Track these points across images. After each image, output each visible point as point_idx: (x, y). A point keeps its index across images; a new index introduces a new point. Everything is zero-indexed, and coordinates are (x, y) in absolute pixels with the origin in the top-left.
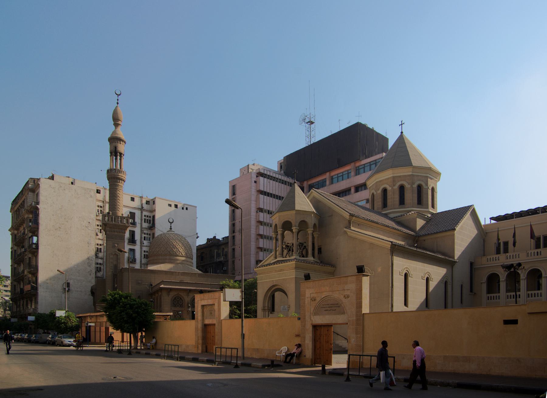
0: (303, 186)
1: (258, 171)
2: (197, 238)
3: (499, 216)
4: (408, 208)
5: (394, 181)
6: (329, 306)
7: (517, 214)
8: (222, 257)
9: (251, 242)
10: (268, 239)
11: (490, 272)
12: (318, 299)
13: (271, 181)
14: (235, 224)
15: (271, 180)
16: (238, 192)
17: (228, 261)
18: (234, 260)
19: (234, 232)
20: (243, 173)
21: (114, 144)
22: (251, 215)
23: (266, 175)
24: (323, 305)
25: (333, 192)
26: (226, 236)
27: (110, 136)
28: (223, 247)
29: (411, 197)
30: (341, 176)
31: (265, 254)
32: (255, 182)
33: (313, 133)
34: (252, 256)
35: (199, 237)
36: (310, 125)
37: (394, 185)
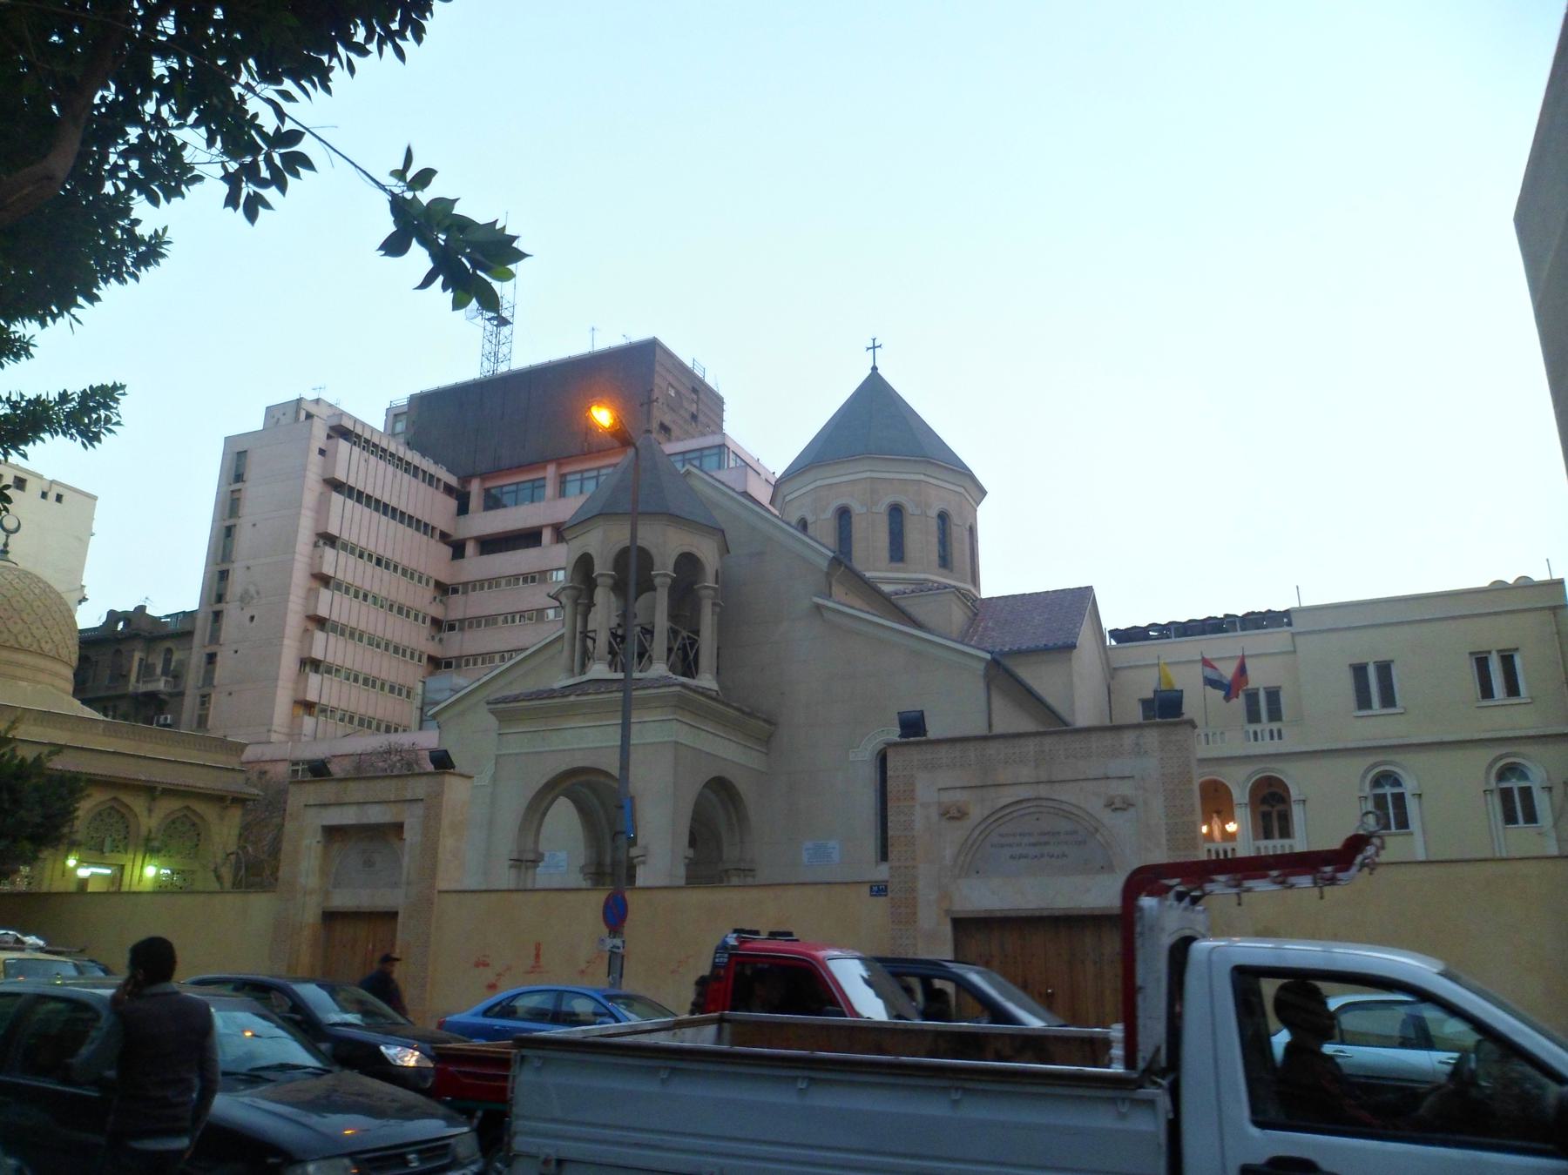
0: (468, 490)
1: (334, 422)
2: (80, 602)
3: (1210, 618)
4: (915, 572)
6: (1032, 840)
7: (1216, 624)
8: (163, 679)
9: (283, 637)
10: (342, 634)
11: (1265, 772)
12: (976, 813)
13: (373, 459)
14: (231, 572)
15: (372, 454)
16: (252, 473)
17: (181, 694)
18: (209, 695)
19: (220, 598)
20: (275, 419)
22: (294, 552)
23: (358, 436)
24: (1001, 835)
26: (187, 610)
28: (168, 644)
30: (513, 492)
31: (327, 683)
32: (322, 452)
33: (504, 350)
34: (280, 683)
35: (87, 599)
36: (497, 326)
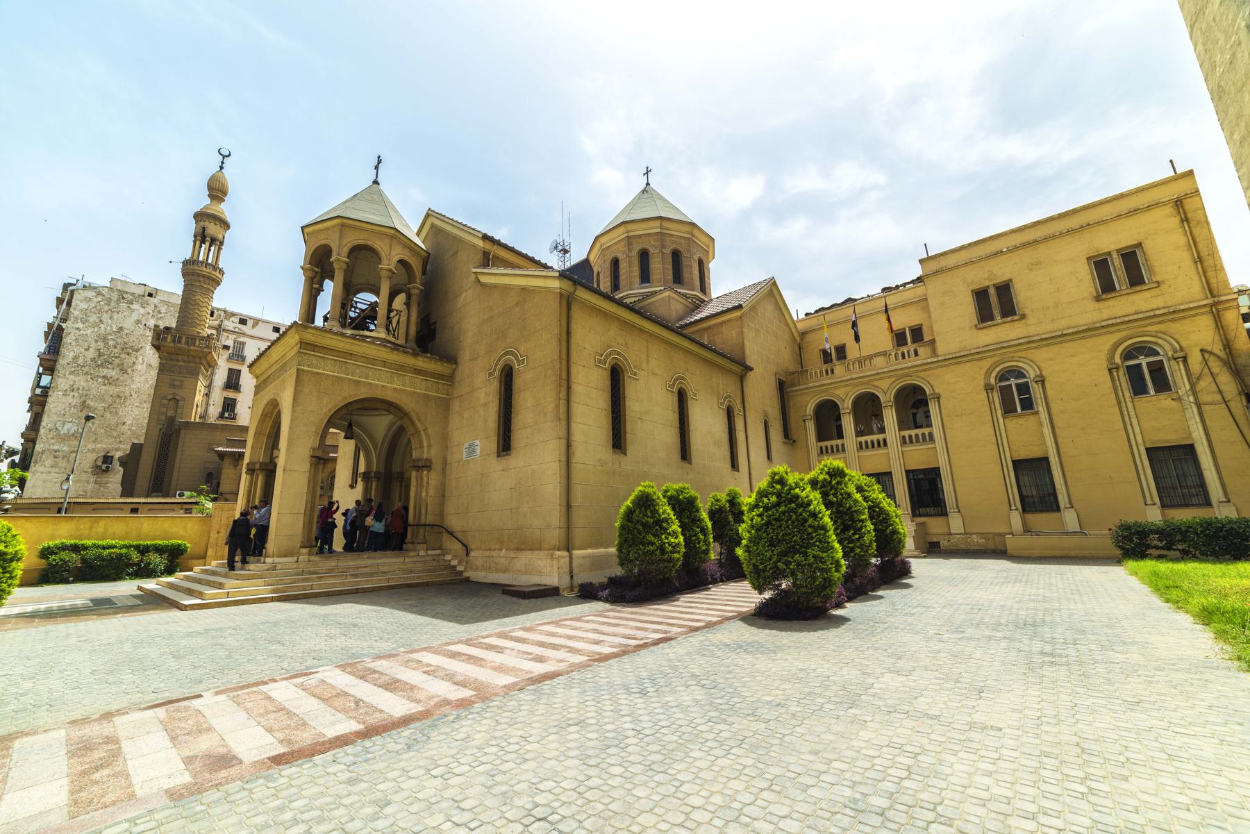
5: (630, 244)
21: (202, 224)
25: (691, 433)
27: (199, 210)
29: (661, 267)
37: (630, 251)
